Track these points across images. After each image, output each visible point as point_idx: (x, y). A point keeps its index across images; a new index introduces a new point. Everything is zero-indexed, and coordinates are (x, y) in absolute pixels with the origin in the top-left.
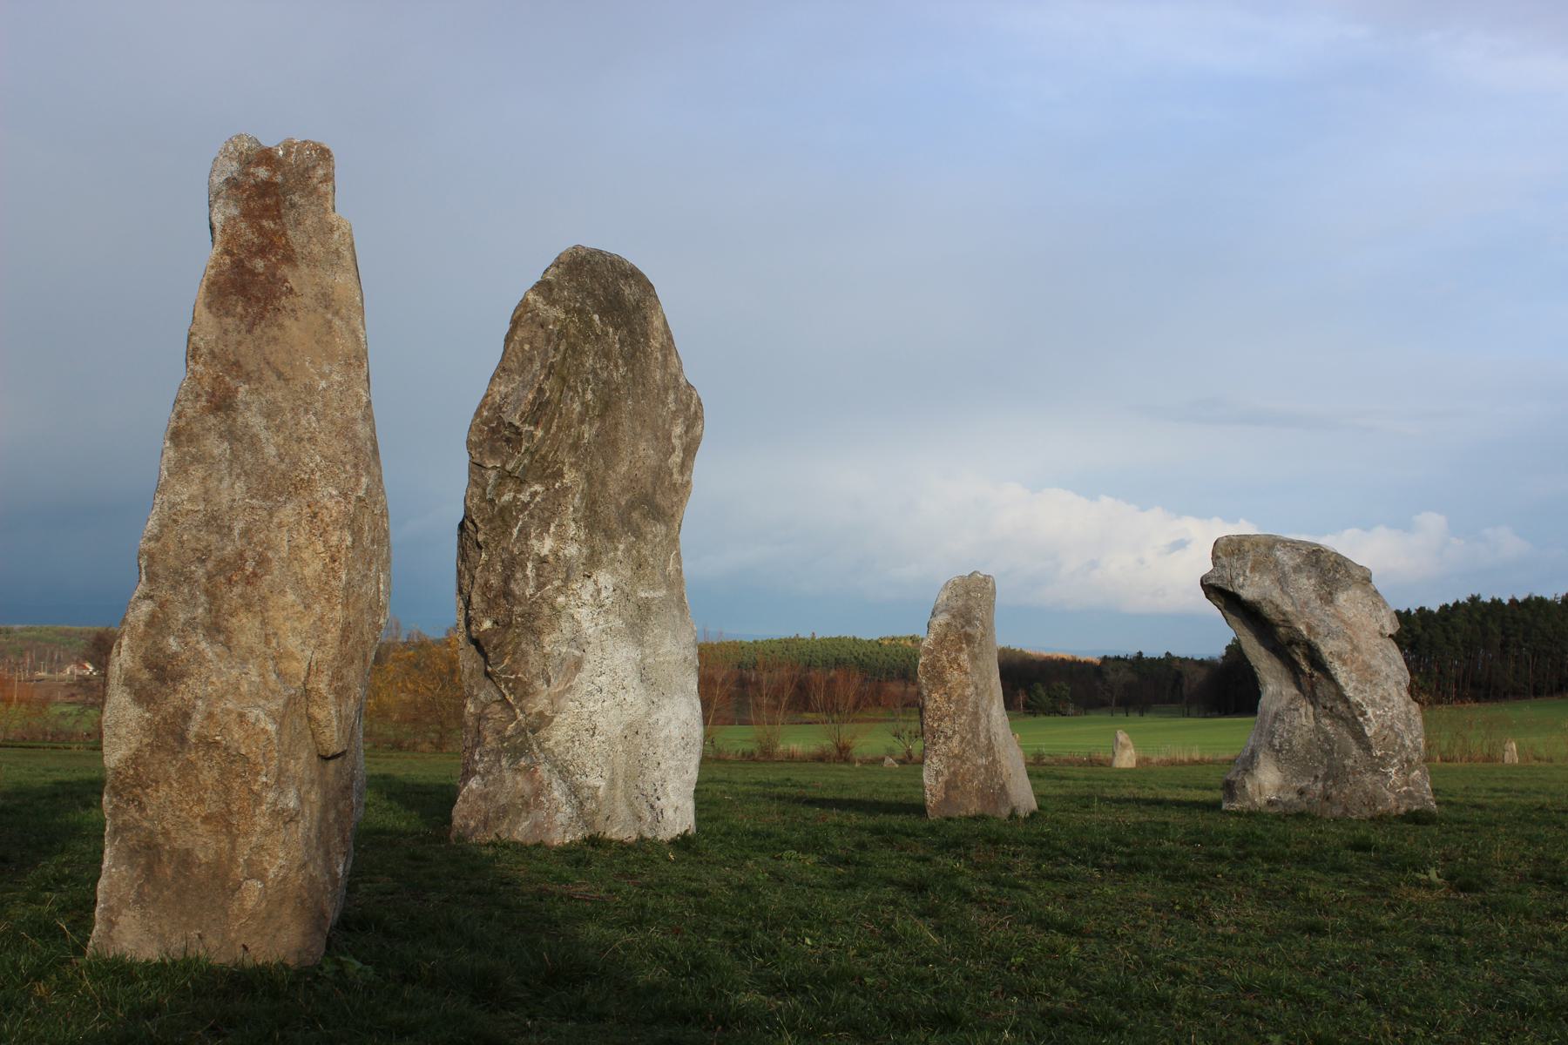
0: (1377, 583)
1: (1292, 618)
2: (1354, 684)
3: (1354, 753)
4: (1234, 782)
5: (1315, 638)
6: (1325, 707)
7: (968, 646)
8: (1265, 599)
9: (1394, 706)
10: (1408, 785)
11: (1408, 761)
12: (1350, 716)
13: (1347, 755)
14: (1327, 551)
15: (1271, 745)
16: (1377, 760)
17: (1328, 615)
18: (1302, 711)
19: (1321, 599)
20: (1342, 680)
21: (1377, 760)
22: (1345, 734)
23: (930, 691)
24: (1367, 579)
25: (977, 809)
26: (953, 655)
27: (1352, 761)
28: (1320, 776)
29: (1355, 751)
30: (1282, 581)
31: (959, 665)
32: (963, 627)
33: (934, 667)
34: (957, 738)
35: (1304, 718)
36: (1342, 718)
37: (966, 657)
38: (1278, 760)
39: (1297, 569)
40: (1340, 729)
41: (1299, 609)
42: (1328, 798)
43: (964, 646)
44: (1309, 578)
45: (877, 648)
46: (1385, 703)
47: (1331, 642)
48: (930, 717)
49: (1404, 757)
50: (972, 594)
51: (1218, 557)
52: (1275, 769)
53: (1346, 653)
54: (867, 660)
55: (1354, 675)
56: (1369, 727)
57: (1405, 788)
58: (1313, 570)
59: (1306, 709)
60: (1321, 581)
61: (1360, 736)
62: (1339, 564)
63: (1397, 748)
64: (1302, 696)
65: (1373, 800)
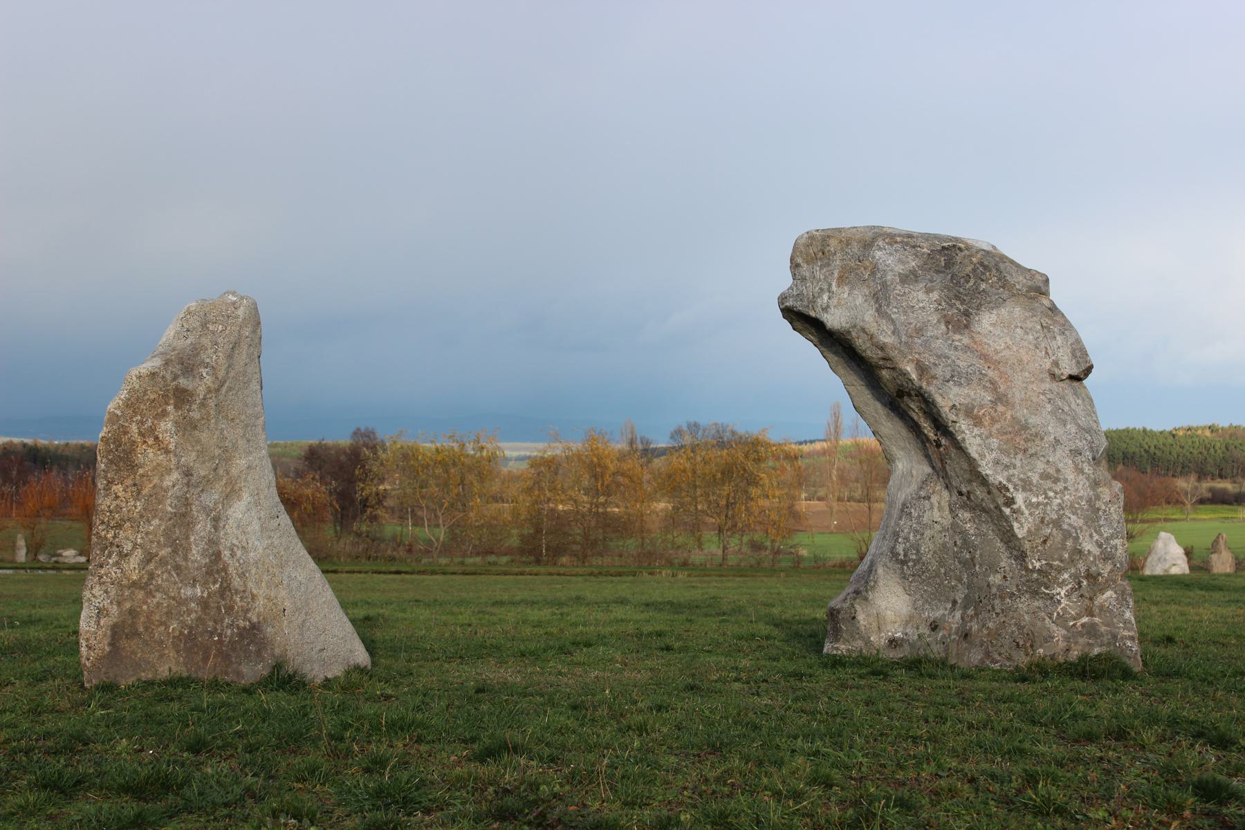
0: (1057, 294)
1: (894, 354)
2: (994, 455)
3: (1003, 564)
4: (839, 612)
5: (928, 384)
6: (960, 494)
7: (177, 407)
8: (855, 326)
9: (1066, 488)
10: (1091, 614)
11: (1092, 577)
12: (992, 506)
13: (993, 568)
14: (968, 248)
15: (894, 554)
16: (1035, 575)
17: (956, 348)
18: (934, 499)
19: (947, 323)
20: (973, 451)
21: (1035, 575)
22: (991, 535)
23: (110, 482)
24: (1038, 288)
25: (174, 669)
26: (149, 423)
27: (999, 576)
28: (959, 601)
29: (1005, 561)
30: (880, 298)
31: (157, 438)
32: (175, 378)
33: (118, 442)
34: (138, 555)
35: (936, 510)
36: (984, 510)
37: (170, 425)
38: (904, 577)
39: (909, 278)
40: (984, 528)
41: (904, 339)
42: (966, 635)
43: (170, 408)
44: (928, 291)
45: (1170, 440)
46: (1049, 484)
47: (956, 390)
48: (103, 523)
49: (1083, 570)
50: (211, 327)
51: (798, 266)
52: (900, 590)
53: (981, 407)
54: (1159, 453)
55: (994, 442)
56: (1019, 522)
57: (1085, 620)
58: (938, 278)
59: (941, 497)
60: (951, 295)
61: (1008, 537)
62: (986, 267)
63: (1066, 556)
64: (935, 477)
65: (1031, 639)
